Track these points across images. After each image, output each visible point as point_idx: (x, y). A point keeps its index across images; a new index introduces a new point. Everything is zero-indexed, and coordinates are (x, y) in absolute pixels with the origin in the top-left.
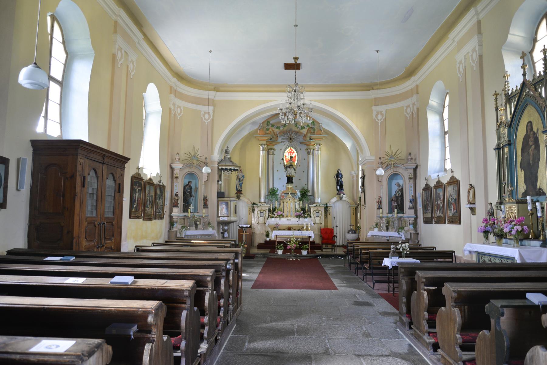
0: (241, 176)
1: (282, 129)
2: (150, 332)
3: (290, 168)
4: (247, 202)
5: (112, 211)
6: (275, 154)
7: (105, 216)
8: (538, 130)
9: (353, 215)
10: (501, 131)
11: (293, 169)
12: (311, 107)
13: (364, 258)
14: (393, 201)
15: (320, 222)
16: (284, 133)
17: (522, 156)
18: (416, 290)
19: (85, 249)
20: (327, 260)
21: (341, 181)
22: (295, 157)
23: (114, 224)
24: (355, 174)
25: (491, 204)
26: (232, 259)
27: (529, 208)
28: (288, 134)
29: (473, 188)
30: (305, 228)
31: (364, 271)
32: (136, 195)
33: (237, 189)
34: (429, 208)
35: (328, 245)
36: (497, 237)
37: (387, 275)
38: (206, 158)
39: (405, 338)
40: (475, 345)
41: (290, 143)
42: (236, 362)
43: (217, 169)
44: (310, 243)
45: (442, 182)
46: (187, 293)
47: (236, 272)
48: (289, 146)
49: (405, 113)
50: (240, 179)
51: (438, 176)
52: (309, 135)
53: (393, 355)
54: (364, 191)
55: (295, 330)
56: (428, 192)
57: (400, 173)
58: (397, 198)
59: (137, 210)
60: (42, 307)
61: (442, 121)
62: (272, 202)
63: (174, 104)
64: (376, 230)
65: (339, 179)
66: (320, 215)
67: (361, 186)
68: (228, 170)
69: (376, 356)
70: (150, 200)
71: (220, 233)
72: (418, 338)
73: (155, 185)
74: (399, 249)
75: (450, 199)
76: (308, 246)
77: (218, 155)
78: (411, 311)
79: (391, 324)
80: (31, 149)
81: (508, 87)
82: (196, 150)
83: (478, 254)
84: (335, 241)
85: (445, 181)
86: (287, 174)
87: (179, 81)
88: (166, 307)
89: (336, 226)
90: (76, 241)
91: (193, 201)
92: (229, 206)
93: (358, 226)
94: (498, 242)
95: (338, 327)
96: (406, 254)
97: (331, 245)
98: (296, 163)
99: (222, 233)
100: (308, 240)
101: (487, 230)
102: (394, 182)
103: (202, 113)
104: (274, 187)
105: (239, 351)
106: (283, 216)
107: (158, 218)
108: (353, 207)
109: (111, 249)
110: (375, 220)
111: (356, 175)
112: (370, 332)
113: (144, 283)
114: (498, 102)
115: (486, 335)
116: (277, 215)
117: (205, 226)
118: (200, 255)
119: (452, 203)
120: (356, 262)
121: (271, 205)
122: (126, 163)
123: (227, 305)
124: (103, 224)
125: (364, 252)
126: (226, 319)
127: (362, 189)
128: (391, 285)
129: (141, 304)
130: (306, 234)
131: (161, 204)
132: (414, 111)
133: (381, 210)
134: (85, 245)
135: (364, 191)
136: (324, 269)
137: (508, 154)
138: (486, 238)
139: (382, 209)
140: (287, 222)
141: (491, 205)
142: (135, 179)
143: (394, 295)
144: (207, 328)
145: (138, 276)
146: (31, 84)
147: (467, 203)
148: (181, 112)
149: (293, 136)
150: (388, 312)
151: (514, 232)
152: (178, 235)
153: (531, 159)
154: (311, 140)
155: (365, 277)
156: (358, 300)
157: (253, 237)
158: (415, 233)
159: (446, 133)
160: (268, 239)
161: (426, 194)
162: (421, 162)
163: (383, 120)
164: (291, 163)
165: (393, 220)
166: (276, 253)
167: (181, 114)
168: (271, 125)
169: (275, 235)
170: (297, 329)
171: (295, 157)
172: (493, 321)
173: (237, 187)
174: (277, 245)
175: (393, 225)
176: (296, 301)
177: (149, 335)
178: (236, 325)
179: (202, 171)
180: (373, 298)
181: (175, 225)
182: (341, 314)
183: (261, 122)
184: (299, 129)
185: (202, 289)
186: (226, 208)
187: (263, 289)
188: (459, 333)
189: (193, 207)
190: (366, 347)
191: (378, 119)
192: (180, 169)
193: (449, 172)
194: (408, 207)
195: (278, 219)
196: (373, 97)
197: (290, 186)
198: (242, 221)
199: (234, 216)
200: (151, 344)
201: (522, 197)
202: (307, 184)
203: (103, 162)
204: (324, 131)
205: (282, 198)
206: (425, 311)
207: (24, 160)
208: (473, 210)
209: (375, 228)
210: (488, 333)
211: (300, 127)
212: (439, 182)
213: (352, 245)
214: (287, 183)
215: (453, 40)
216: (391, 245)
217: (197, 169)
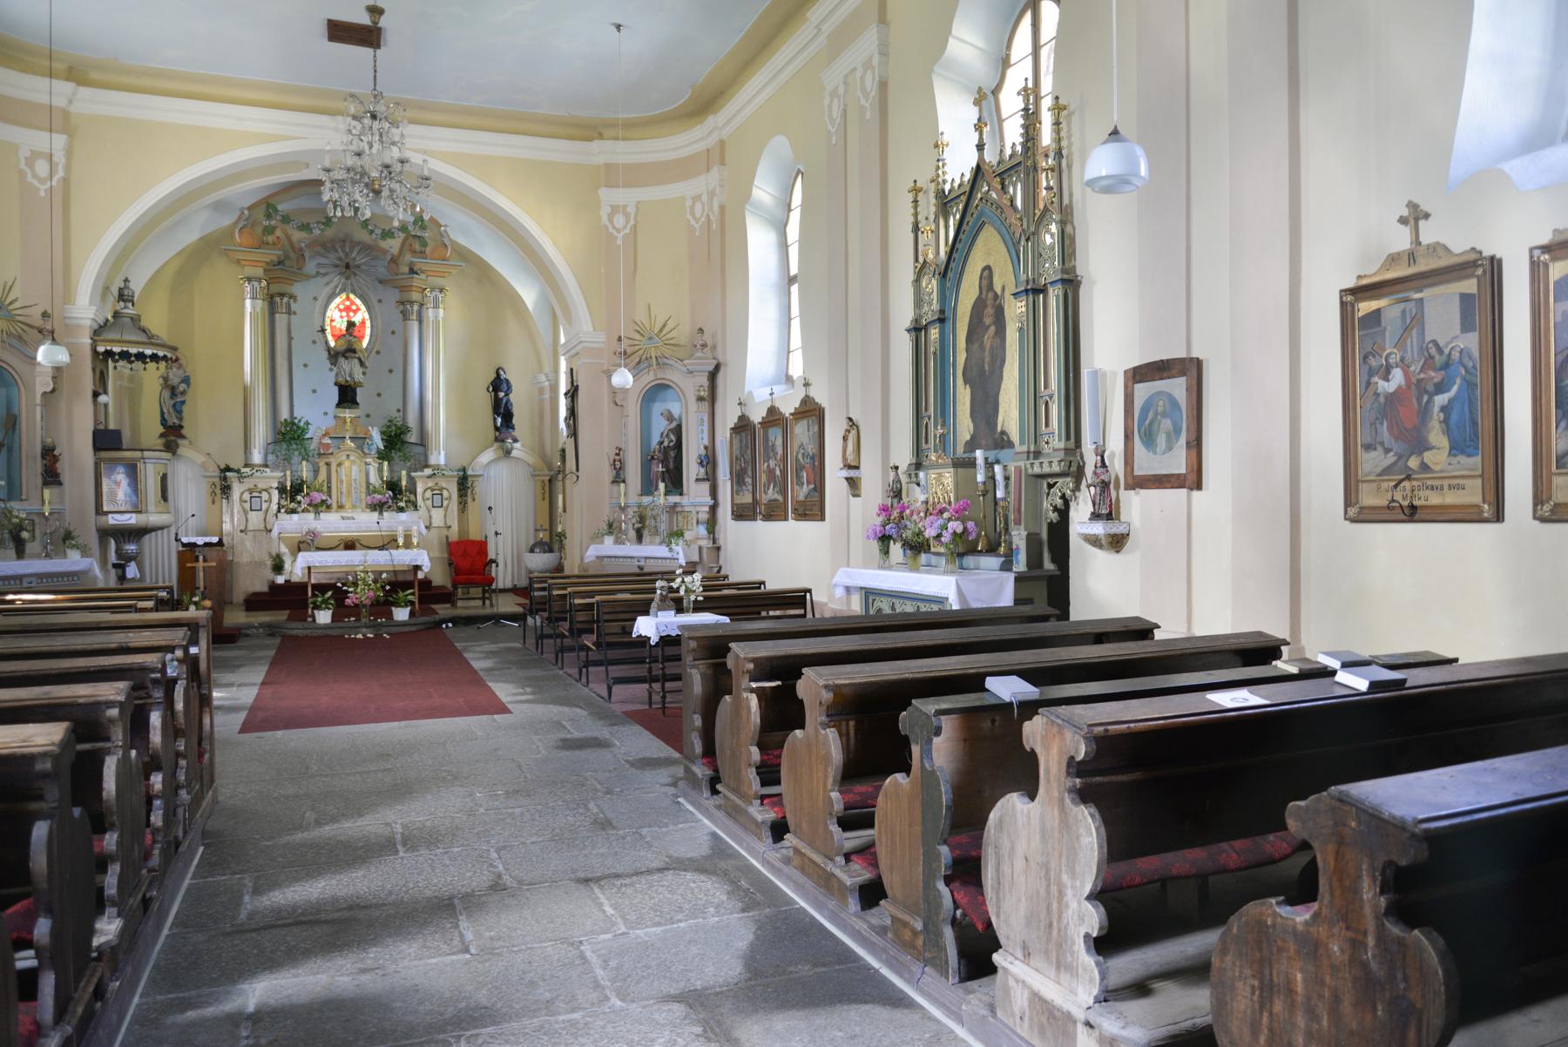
1: (317, 232)
3: (346, 358)
4: (203, 463)
8: (1003, 289)
9: (544, 499)
10: (924, 285)
11: (356, 361)
12: (426, 173)
15: (446, 523)
16: (323, 245)
17: (967, 350)
18: (730, 693)
20: (470, 631)
21: (508, 401)
22: (363, 322)
24: (547, 383)
25: (897, 468)
27: (980, 478)
28: (339, 249)
31: (583, 654)
33: (164, 421)
34: (748, 480)
35: (471, 590)
36: (911, 549)
37: (645, 662)
38: (45, 315)
39: (700, 820)
40: (874, 813)
41: (347, 278)
43: (88, 353)
44: (416, 584)
47: (195, 684)
48: (341, 291)
49: (688, 216)
52: (408, 257)
54: (574, 433)
55: (398, 837)
56: (747, 437)
57: (677, 386)
58: (666, 451)
61: (784, 246)
62: (289, 463)
64: (609, 540)
65: (501, 394)
66: (445, 503)
67: (566, 419)
68: (133, 359)
69: (632, 875)
71: (110, 566)
74: (677, 591)
75: (800, 457)
76: (412, 595)
77: (91, 303)
84: (493, 574)
85: (788, 408)
86: (337, 375)
89: (497, 534)
92: (141, 476)
93: (559, 530)
94: (911, 561)
95: (522, 814)
96: (696, 601)
97: (480, 589)
98: (365, 343)
100: (410, 578)
101: (887, 533)
102: (658, 408)
103: (24, 153)
106: (329, 507)
108: (543, 478)
110: (606, 513)
111: (551, 385)
112: (610, 815)
114: (919, 209)
116: (309, 505)
117: (51, 544)
118: (61, 639)
120: (557, 632)
121: (288, 473)
123: (172, 787)
125: (579, 604)
127: (568, 426)
128: (657, 686)
130: (403, 558)
132: (713, 213)
133: (622, 485)
135: (574, 433)
136: (465, 659)
139: (624, 481)
140: (343, 525)
143: (664, 714)
144: (114, 870)
147: (842, 466)
149: (354, 259)
150: (653, 759)
151: (946, 537)
153: (987, 360)
155: (584, 670)
156: (569, 736)
158: (711, 545)
159: (792, 280)
160: (280, 580)
161: (741, 441)
162: (728, 356)
163: (627, 231)
165: (654, 513)
166: (310, 619)
168: (279, 218)
169: (305, 565)
171: (363, 322)
172: (916, 750)
173: (166, 416)
174: (314, 595)
175: (655, 527)
176: (389, 755)
178: (201, 849)
182: (526, 777)
184: (374, 236)
185: (101, 745)
186: (129, 485)
187: (280, 732)
188: (836, 788)
190: (603, 854)
191: (614, 227)
194: (693, 477)
195: (311, 516)
196: (600, 160)
197: (348, 414)
198: (187, 527)
199: (160, 509)
202: (401, 407)
204: (454, 250)
205: (322, 452)
208: (853, 483)
209: (607, 534)
210: (904, 778)
211: (378, 231)
212: (772, 410)
214: (339, 405)
215: (818, 27)
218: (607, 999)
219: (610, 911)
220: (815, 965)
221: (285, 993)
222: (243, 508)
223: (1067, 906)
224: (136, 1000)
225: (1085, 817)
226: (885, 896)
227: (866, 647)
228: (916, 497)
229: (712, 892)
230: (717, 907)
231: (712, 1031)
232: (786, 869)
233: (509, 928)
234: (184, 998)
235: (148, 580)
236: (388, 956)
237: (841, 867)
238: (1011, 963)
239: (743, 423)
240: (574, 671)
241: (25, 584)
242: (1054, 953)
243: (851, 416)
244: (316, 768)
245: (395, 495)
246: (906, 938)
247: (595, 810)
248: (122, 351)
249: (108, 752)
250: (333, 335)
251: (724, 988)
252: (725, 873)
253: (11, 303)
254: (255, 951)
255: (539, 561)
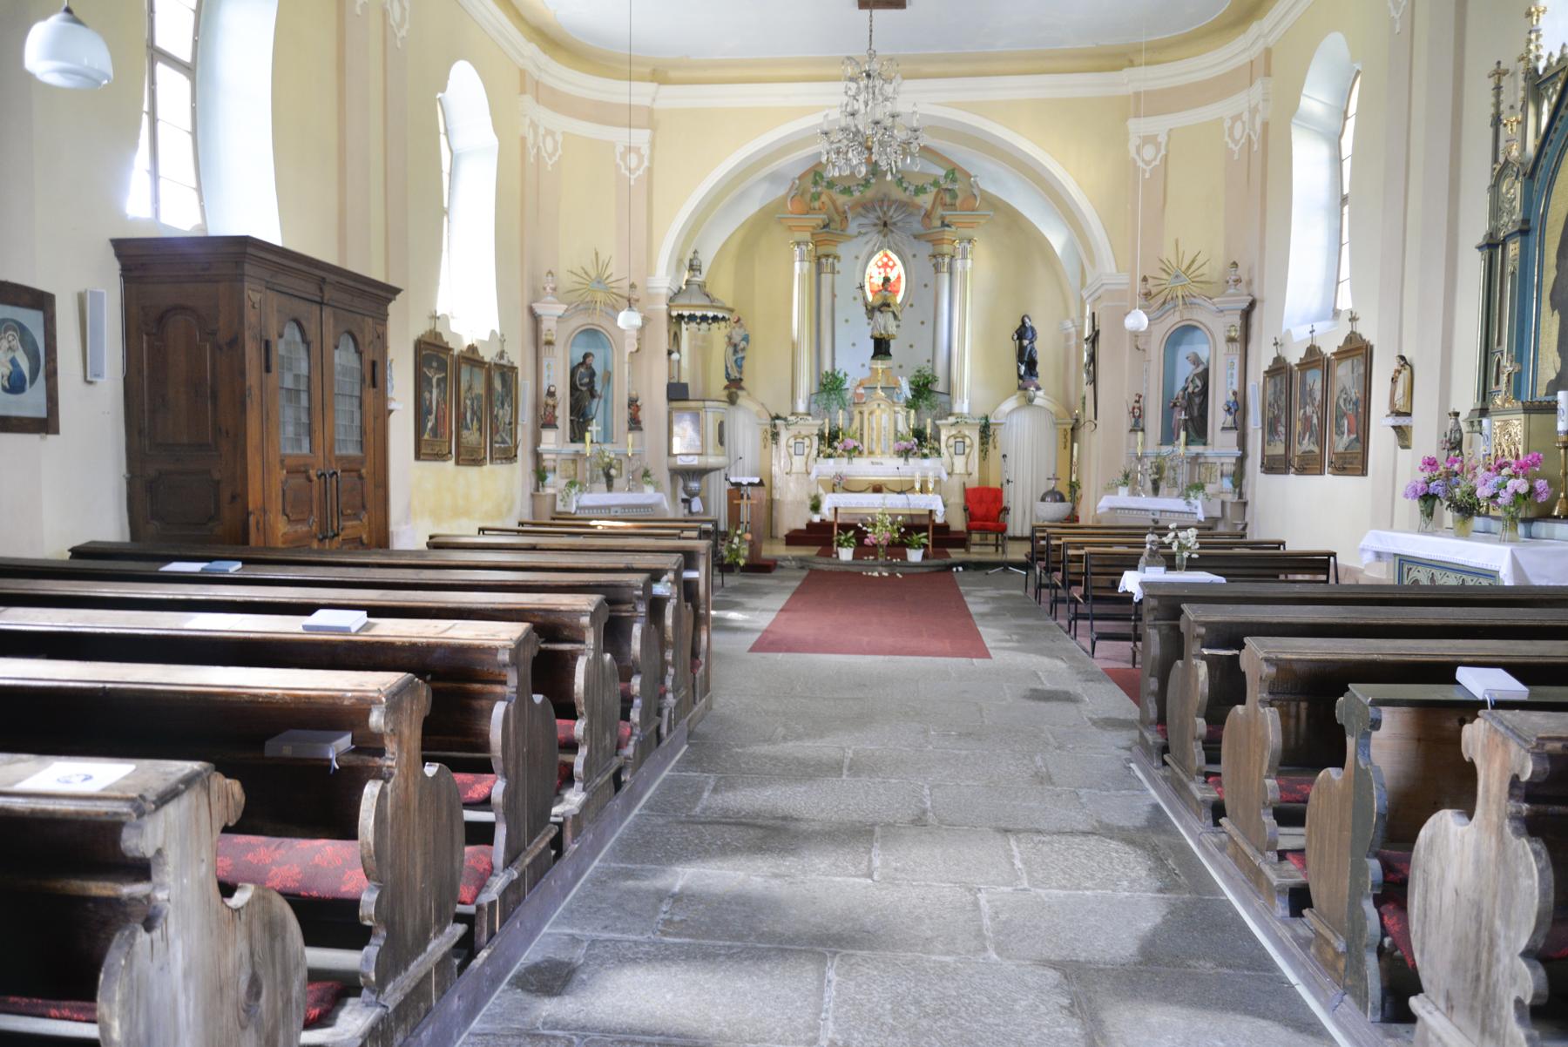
1: (857, 194)
2: (380, 752)
3: (881, 312)
5: (356, 437)
6: (838, 272)
7: (337, 453)
9: (1065, 448)
10: (1504, 190)
11: (891, 315)
13: (1072, 570)
14: (1178, 409)
16: (864, 206)
17: (1558, 267)
19: (284, 543)
20: (979, 575)
21: (1032, 349)
22: (899, 277)
23: (364, 475)
24: (1073, 330)
25: (1457, 414)
28: (878, 209)
29: (1407, 367)
30: (917, 487)
32: (431, 393)
33: (728, 376)
35: (989, 536)
37: (1130, 620)
41: (885, 236)
44: (931, 528)
45: (1322, 349)
46: (504, 657)
47: (689, 605)
48: (880, 249)
49: (1227, 139)
50: (735, 346)
51: (1312, 332)
52: (940, 211)
53: (1101, 831)
55: (847, 762)
56: (1281, 380)
57: (1201, 323)
60: (101, 685)
61: (1338, 160)
63: (534, 125)
64: (1123, 492)
65: (1026, 342)
66: (967, 450)
69: (1054, 833)
70: (473, 409)
71: (679, 501)
72: (1179, 789)
74: (1169, 546)
77: (667, 274)
78: (1168, 714)
79: (1118, 752)
80: (115, 266)
81: (1537, 47)
83: (1400, 560)
85: (1329, 348)
87: (545, 53)
90: (258, 523)
96: (1189, 558)
98: (899, 299)
99: (684, 501)
100: (925, 521)
101: (1431, 492)
102: (1184, 351)
103: (620, 149)
104: (834, 369)
107: (500, 459)
109: (358, 543)
110: (1123, 464)
111: (1077, 331)
114: (1502, 97)
115: (1333, 781)
119: (1345, 414)
121: (827, 421)
122: (390, 300)
124: (331, 476)
126: (653, 727)
130: (931, 503)
131: (507, 421)
133: (1140, 434)
134: (285, 534)
136: (964, 602)
137: (1517, 263)
138: (1428, 516)
139: (1143, 430)
141: (1456, 420)
142: (426, 349)
144: (583, 751)
145: (375, 611)
147: (1388, 412)
148: (555, 149)
149: (891, 217)
150: (1120, 720)
151: (1505, 498)
152: (560, 507)
154: (947, 229)
155: (1073, 623)
156: (1040, 687)
157: (774, 514)
159: (1344, 200)
160: (816, 519)
161: (1276, 386)
163: (1157, 162)
164: (885, 298)
165: (1174, 463)
166: (834, 556)
167: (557, 155)
168: (824, 184)
169: (832, 506)
170: (851, 759)
171: (899, 277)
172: (1351, 742)
174: (839, 534)
175: (1174, 479)
176: (865, 685)
177: (379, 761)
178: (686, 747)
180: (1087, 680)
181: (551, 478)
182: (983, 722)
183: (797, 176)
184: (908, 193)
187: (780, 655)
188: (1273, 775)
192: (559, 317)
193: (1345, 318)
194: (1219, 426)
195: (845, 460)
196: (1130, 89)
197: (880, 365)
200: (380, 783)
201: (1547, 395)
203: (318, 299)
204: (983, 199)
206: (1197, 716)
207: (98, 297)
208: (1402, 434)
209: (1121, 485)
211: (912, 188)
212: (1312, 351)
213: (1045, 534)
214: (874, 357)
216: (1146, 534)
218: (985, 949)
219: (1018, 864)
220: (1221, 965)
221: (707, 881)
223: (1498, 960)
225: (1526, 854)
226: (1310, 905)
227: (1349, 621)
228: (1478, 449)
229: (1132, 865)
230: (1132, 881)
231: (1080, 1006)
232: (1219, 856)
233: (915, 862)
235: (712, 514)
237: (1271, 864)
238: (1430, 1013)
239: (1279, 366)
240: (1065, 623)
241: (612, 513)
242: (1480, 1013)
243: (1403, 354)
244: (799, 690)
245: (920, 442)
246: (1329, 957)
247: (1040, 763)
250: (872, 291)
251: (1109, 966)
252: (1154, 848)
255: (1053, 510)
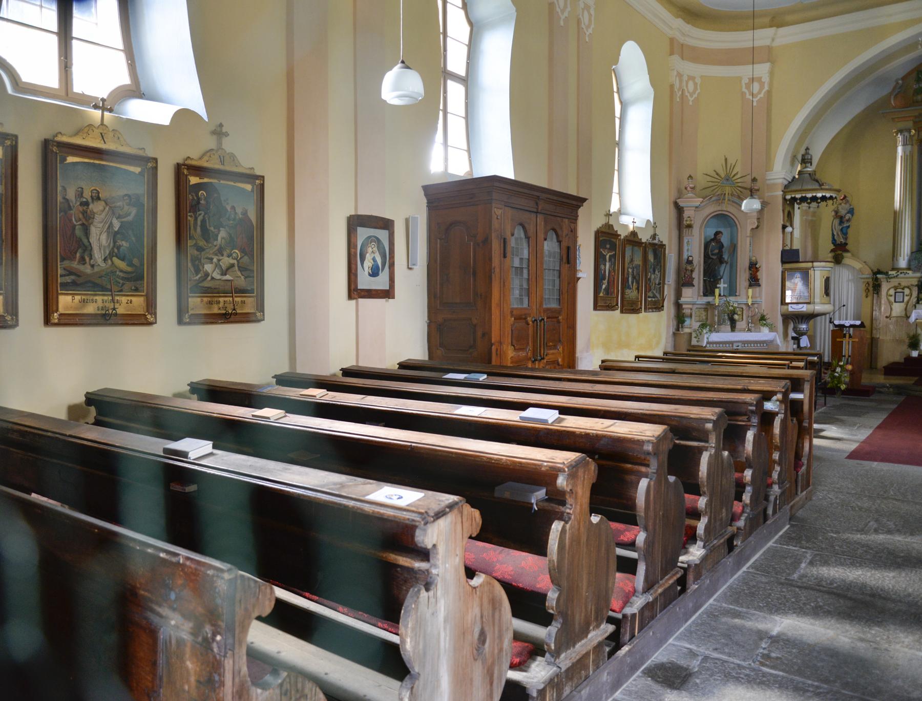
0: (846, 212)
19: (512, 363)
23: (561, 321)
26: (780, 392)
33: (834, 241)
42: (770, 594)
46: (649, 448)
59: (608, 295)
60: (409, 444)
63: (680, 75)
68: (819, 201)
71: (790, 338)
73: (644, 245)
82: (731, 164)
87: (688, 23)
88: (595, 467)
91: (726, 272)
99: (793, 338)
103: (745, 81)
105: (782, 576)
107: (652, 308)
109: (555, 365)
113: (574, 423)
122: (579, 207)
129: (549, 456)
131: (657, 282)
134: (512, 357)
142: (603, 236)
145: (565, 411)
146: (399, 97)
167: (697, 93)
177: (562, 509)
178: (788, 526)
179: (741, 206)
181: (688, 322)
183: (900, 77)
187: (876, 463)
189: (726, 285)
199: (823, 301)
203: (535, 210)
207: (415, 219)
217: (734, 204)
221: (800, 632)
222: (888, 300)
224: (711, 601)
234: (737, 610)
236: (885, 637)
248: (802, 196)
249: (706, 449)
253: (734, 176)
254: (793, 600)
